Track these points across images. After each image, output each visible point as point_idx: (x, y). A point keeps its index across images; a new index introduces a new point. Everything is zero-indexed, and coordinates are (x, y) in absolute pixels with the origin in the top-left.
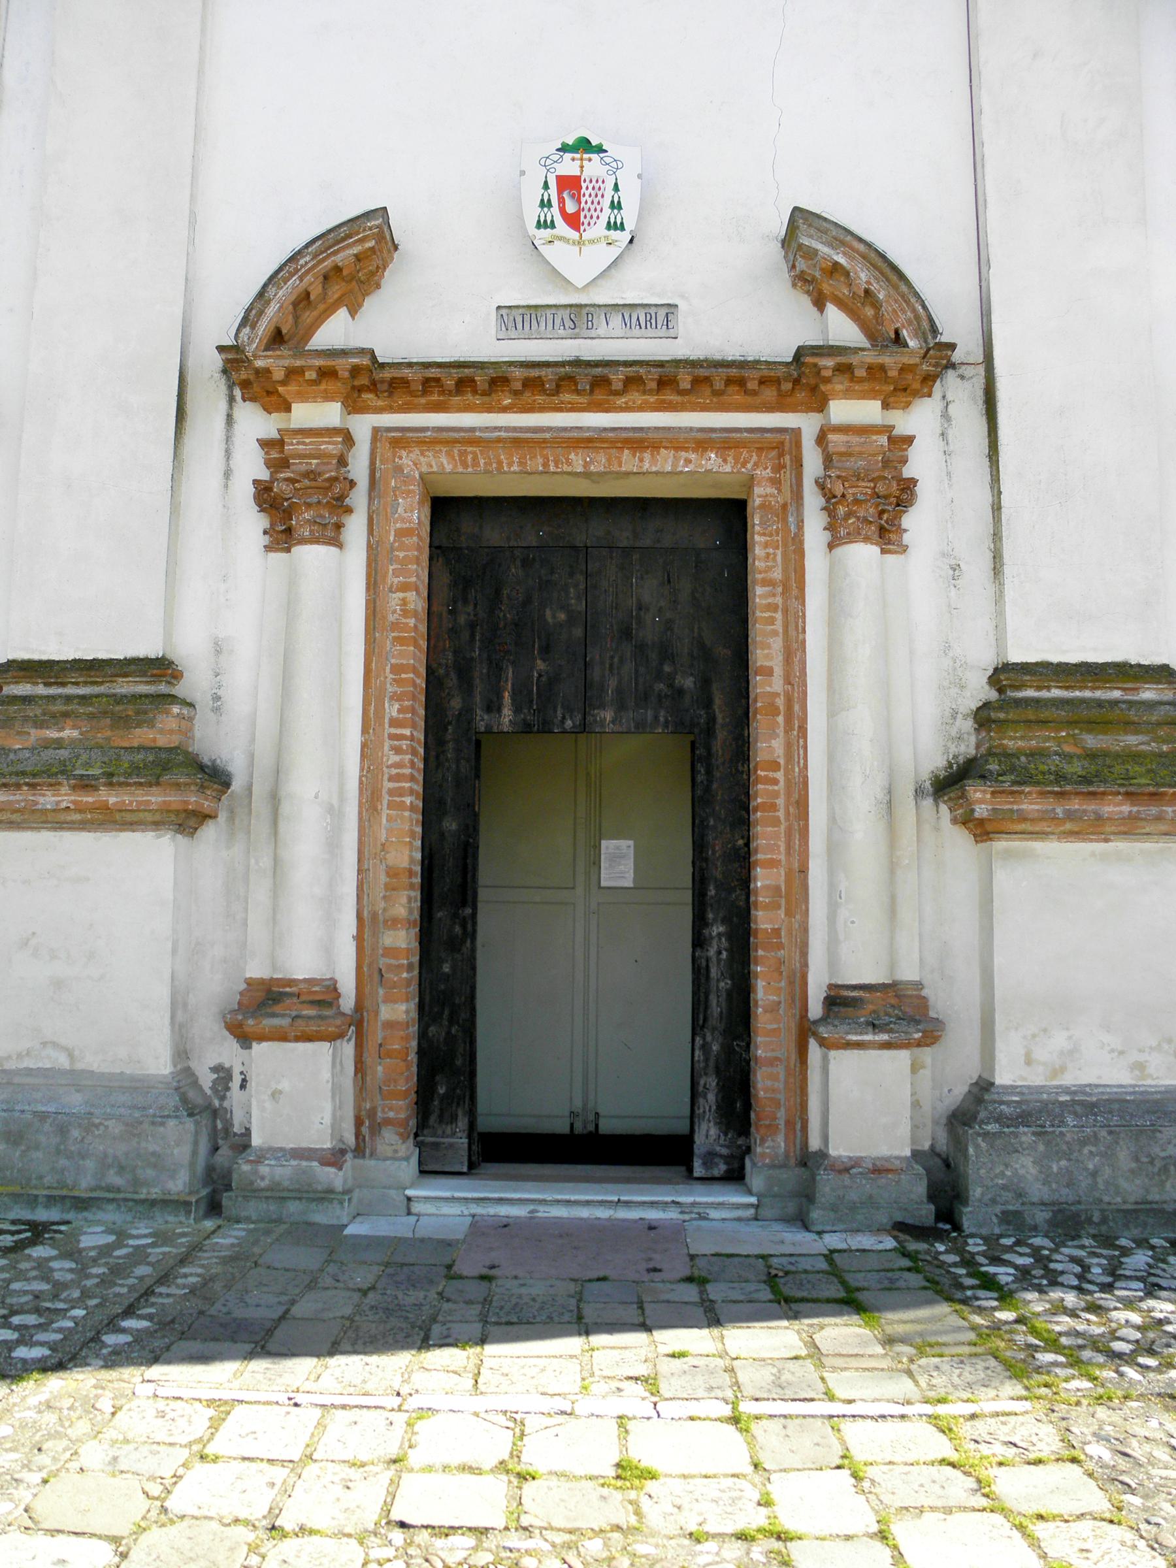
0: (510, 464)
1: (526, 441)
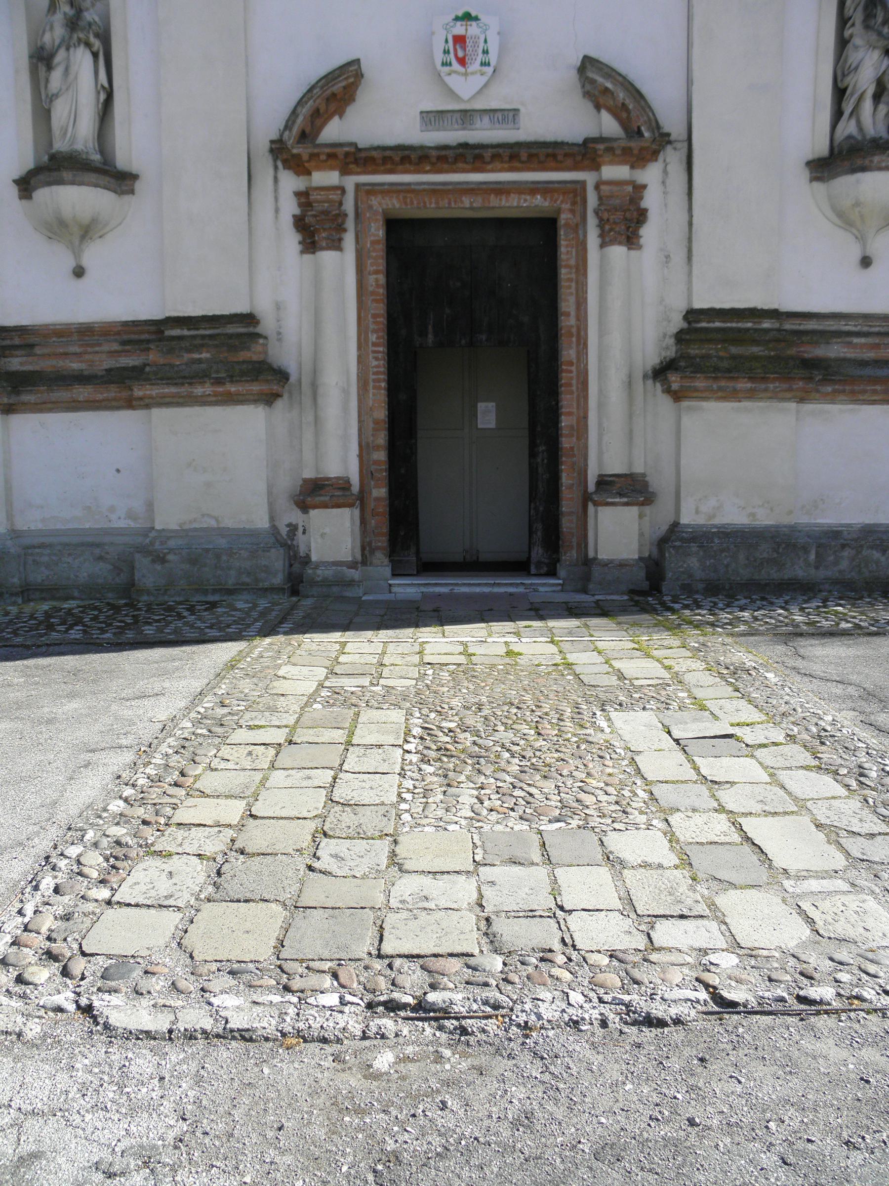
0: (431, 203)
1: (438, 190)
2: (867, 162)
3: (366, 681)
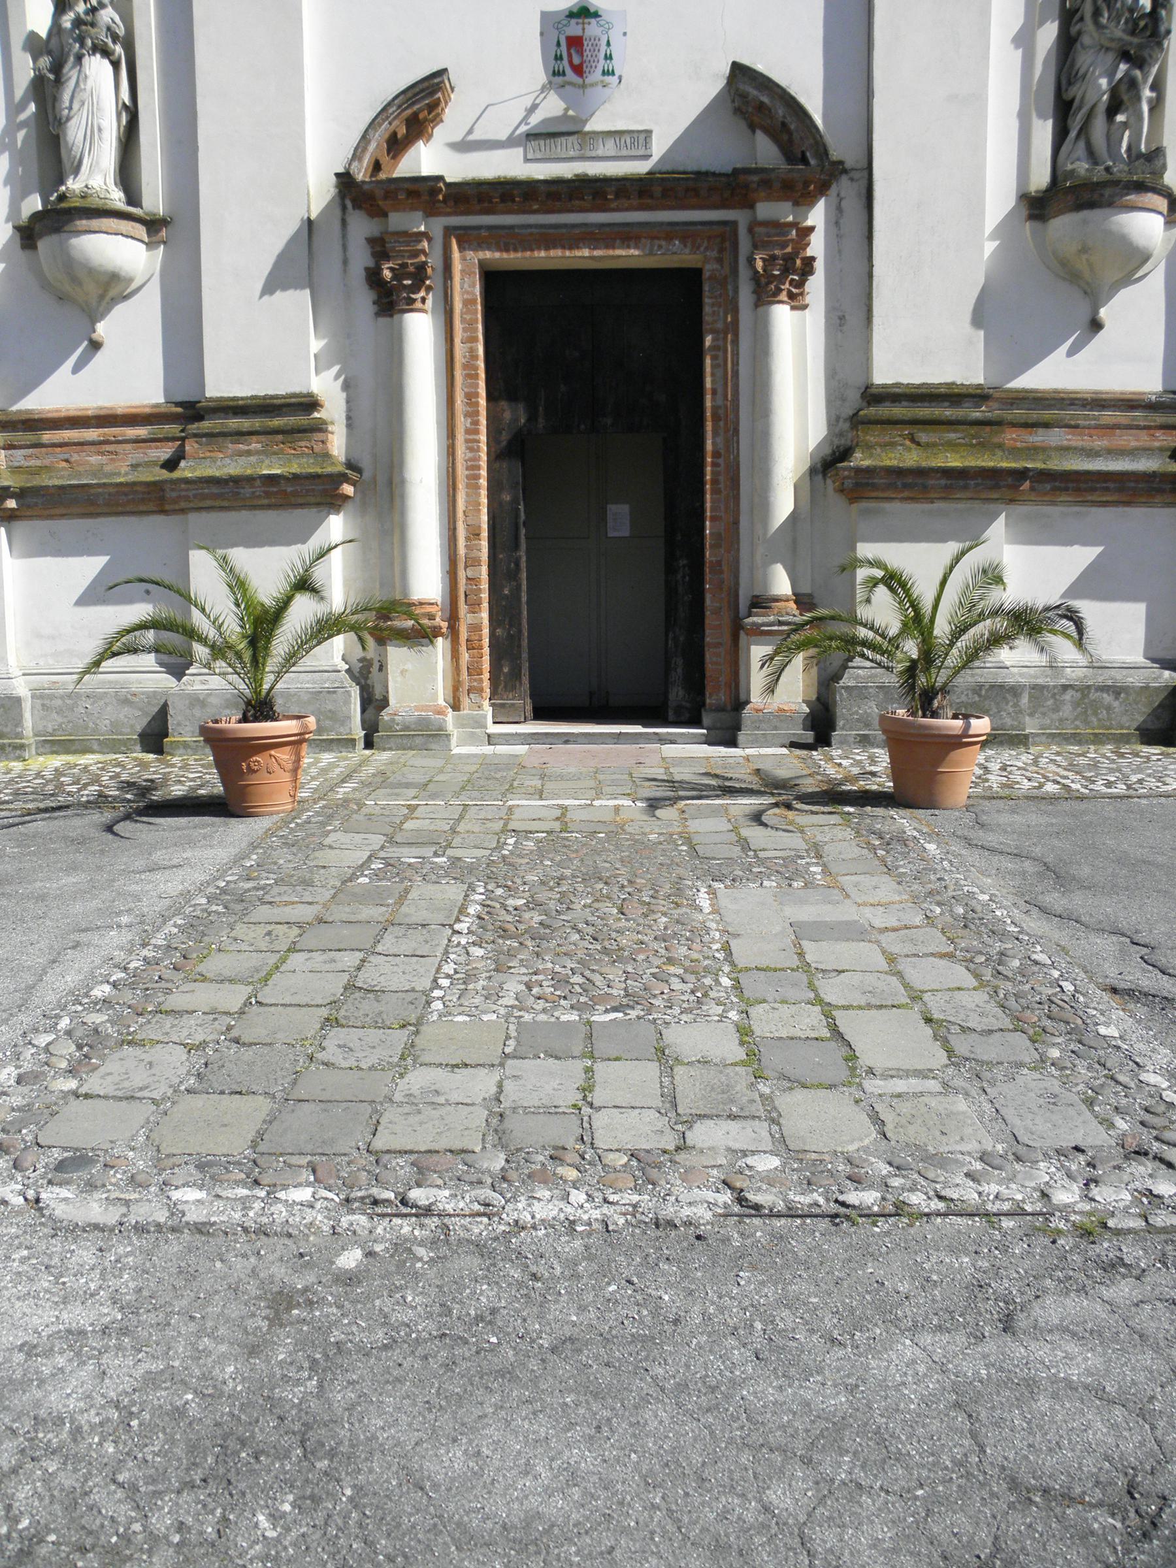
2: (1096, 196)
3: (428, 851)
